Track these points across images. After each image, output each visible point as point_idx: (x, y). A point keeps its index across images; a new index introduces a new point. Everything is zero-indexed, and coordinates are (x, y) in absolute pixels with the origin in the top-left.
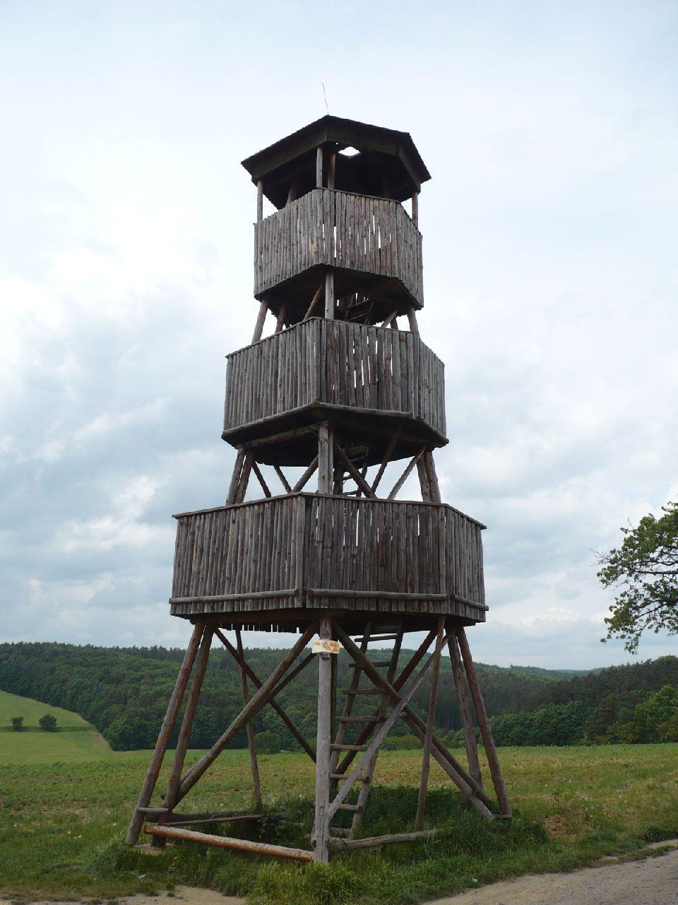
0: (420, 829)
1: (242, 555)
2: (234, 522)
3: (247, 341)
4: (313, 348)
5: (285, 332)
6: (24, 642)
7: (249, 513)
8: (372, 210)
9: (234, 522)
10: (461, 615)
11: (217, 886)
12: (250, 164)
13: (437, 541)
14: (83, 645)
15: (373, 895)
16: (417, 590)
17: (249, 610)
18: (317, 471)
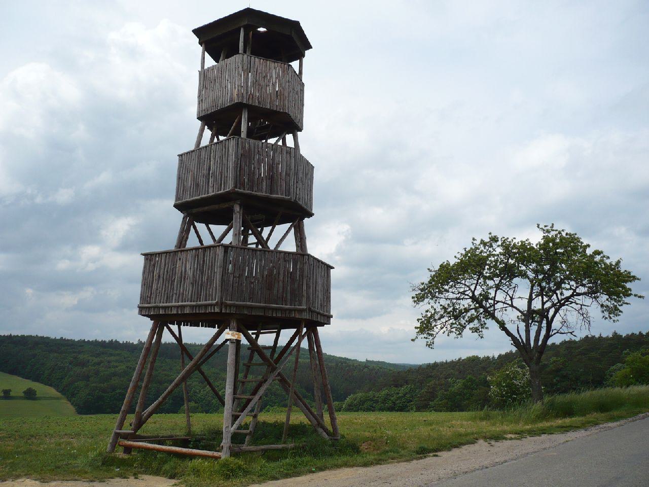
0: (285, 443)
1: (184, 279)
2: (180, 259)
3: (192, 147)
4: (232, 156)
5: (216, 143)
6: (13, 334)
7: (190, 255)
8: (274, 69)
9: (180, 259)
10: (315, 319)
11: (164, 474)
12: (198, 32)
13: (302, 275)
14: (58, 338)
15: (255, 475)
16: (289, 303)
17: (188, 312)
18: (232, 230)
